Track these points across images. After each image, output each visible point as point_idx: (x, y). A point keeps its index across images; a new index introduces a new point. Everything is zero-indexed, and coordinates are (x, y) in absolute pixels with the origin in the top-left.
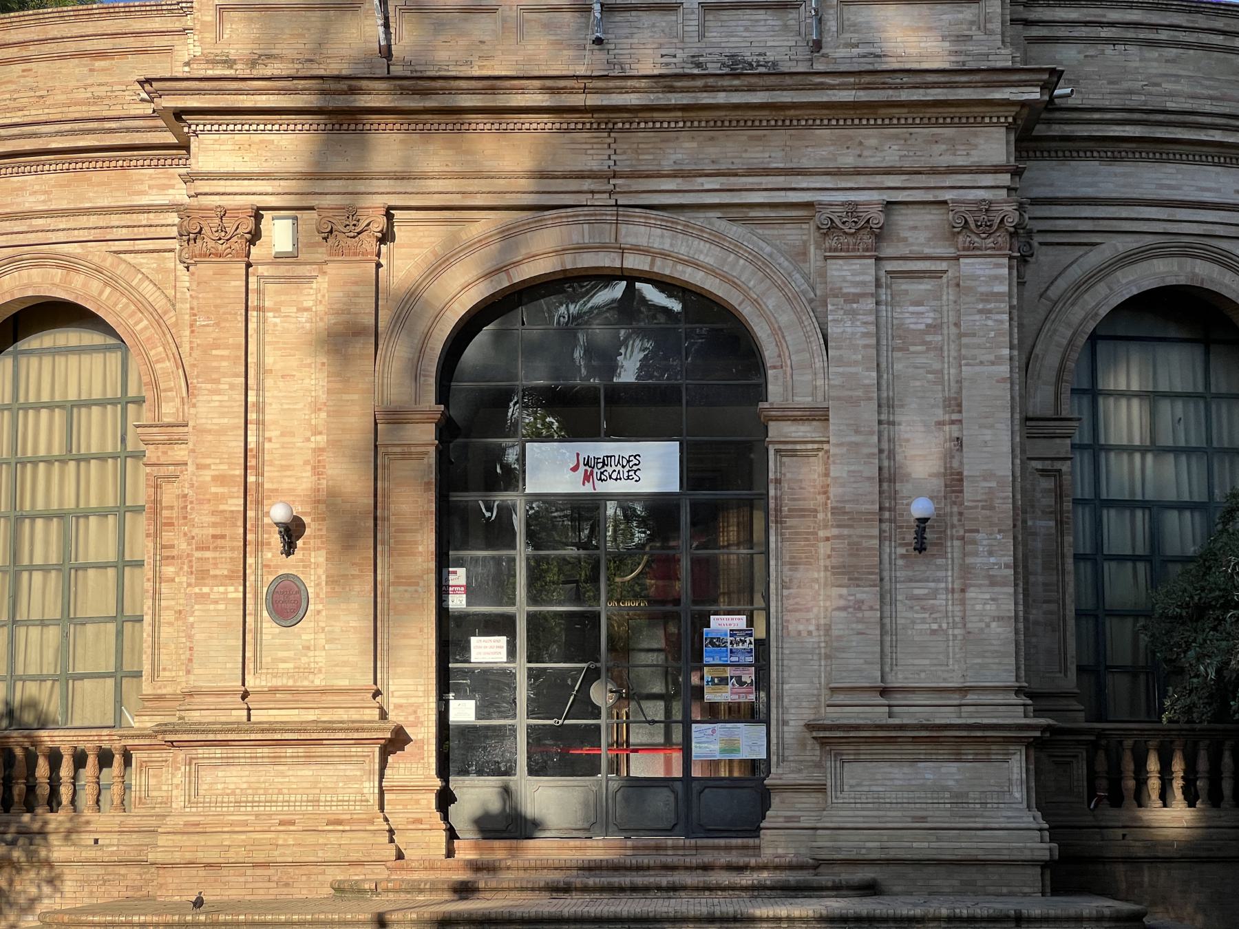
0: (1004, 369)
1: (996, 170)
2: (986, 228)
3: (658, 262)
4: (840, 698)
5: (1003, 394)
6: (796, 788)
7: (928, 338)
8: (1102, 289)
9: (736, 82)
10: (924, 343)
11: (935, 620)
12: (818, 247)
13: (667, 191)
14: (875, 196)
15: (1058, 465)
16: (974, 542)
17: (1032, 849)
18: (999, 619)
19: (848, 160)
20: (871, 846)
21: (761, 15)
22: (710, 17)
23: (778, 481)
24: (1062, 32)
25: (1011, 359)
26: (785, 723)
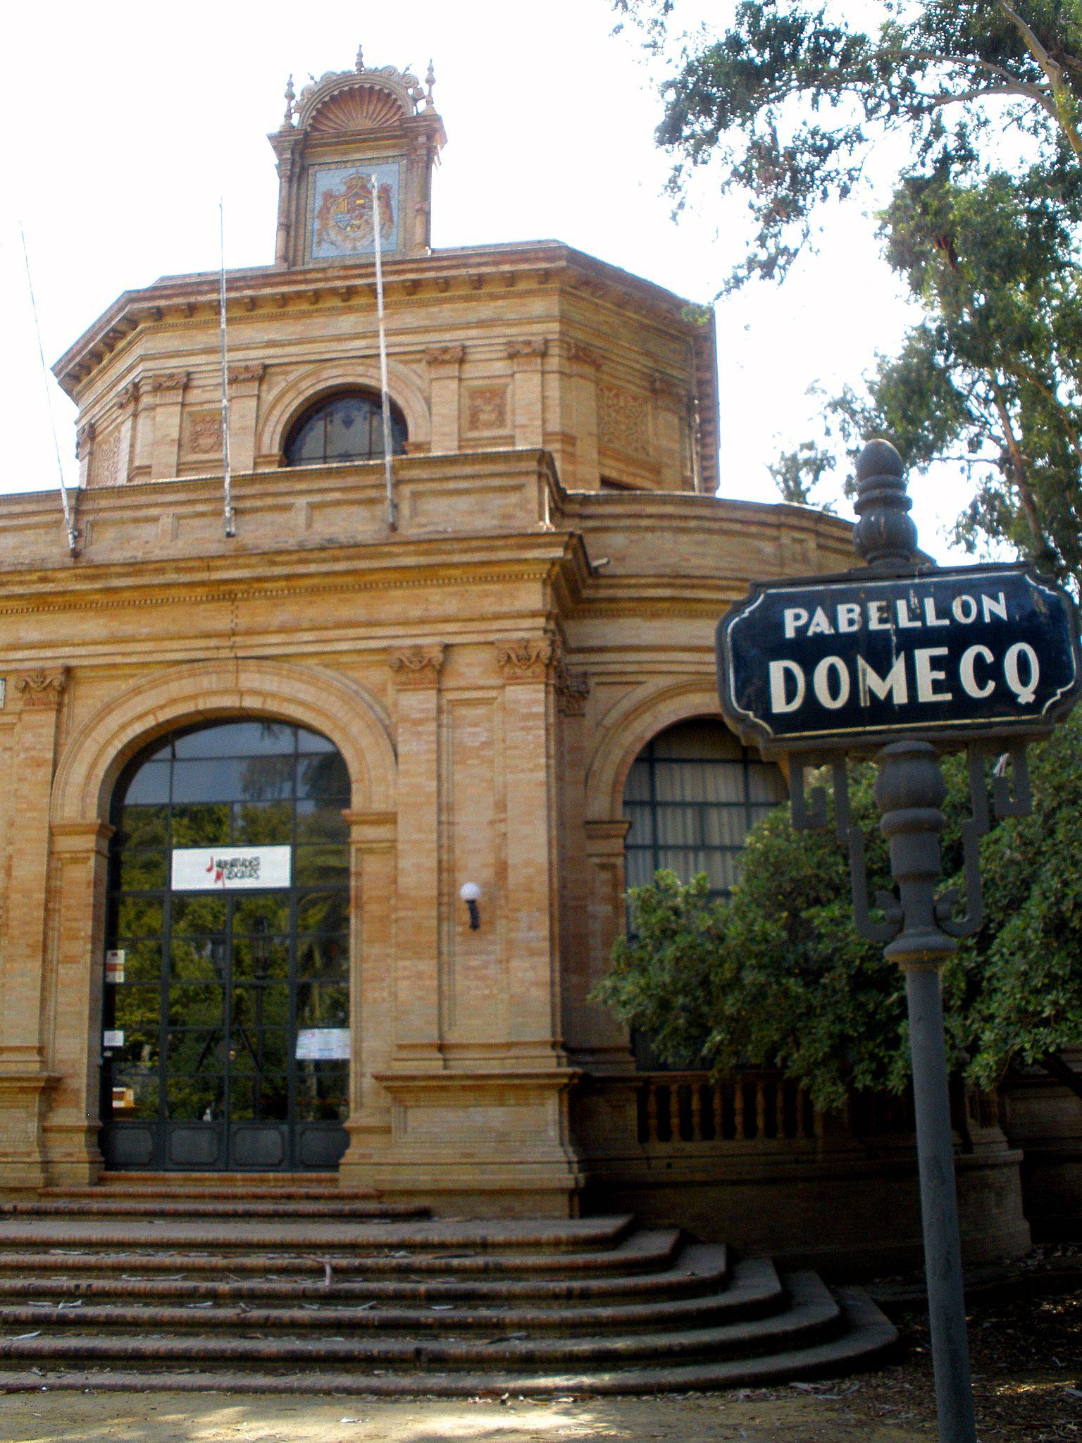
0: (541, 775)
1: (534, 614)
2: (525, 660)
3: (269, 701)
4: (404, 1054)
5: (541, 794)
6: (369, 1130)
7: (483, 753)
8: (647, 718)
9: (323, 555)
10: (478, 757)
11: (487, 987)
12: (395, 683)
13: (273, 644)
14: (437, 639)
15: (613, 860)
16: (516, 920)
17: (559, 1180)
18: (537, 984)
19: (416, 612)
20: (424, 1179)
21: (355, 509)
22: (316, 513)
23: (359, 875)
24: (611, 523)
25: (548, 766)
26: (363, 1075)
